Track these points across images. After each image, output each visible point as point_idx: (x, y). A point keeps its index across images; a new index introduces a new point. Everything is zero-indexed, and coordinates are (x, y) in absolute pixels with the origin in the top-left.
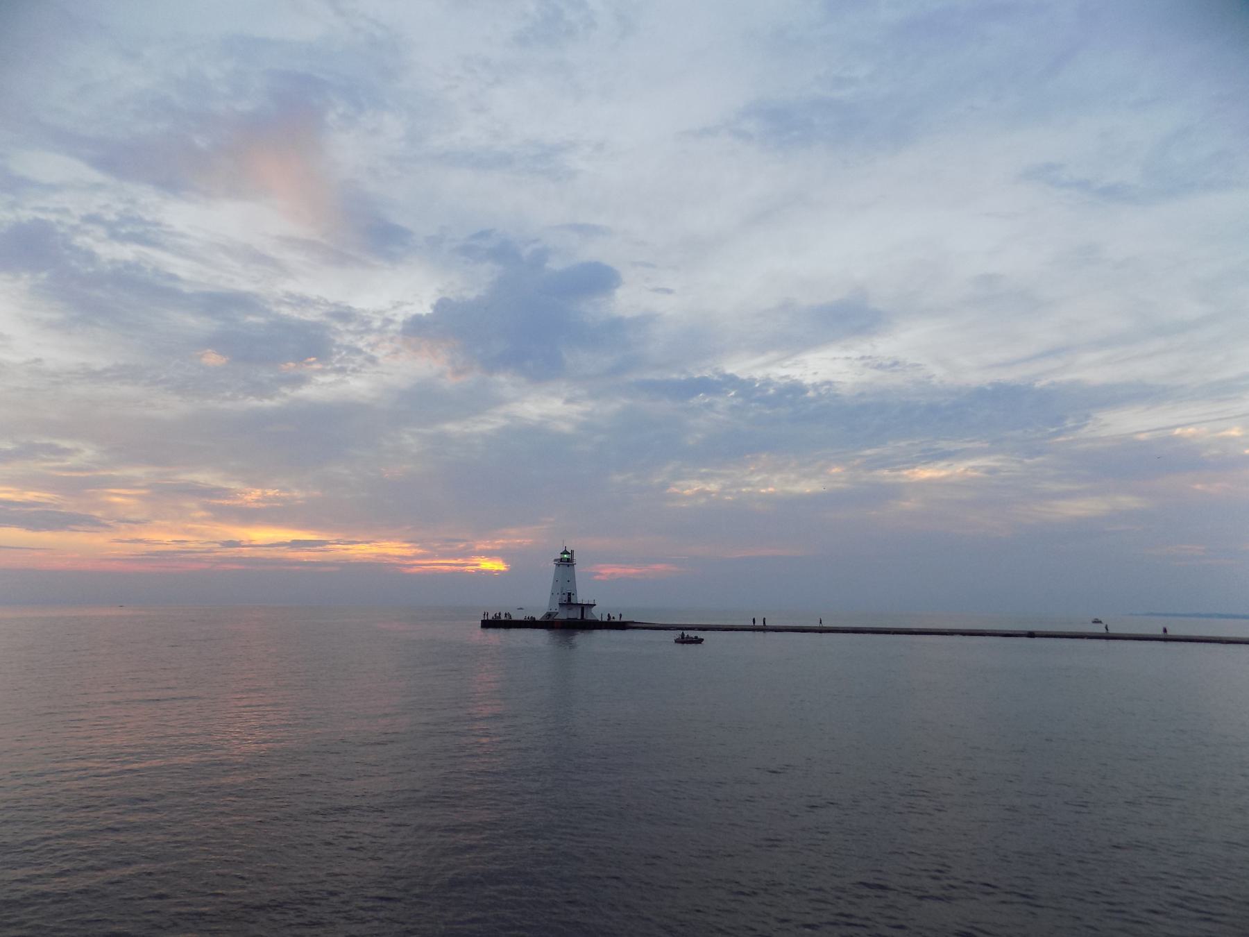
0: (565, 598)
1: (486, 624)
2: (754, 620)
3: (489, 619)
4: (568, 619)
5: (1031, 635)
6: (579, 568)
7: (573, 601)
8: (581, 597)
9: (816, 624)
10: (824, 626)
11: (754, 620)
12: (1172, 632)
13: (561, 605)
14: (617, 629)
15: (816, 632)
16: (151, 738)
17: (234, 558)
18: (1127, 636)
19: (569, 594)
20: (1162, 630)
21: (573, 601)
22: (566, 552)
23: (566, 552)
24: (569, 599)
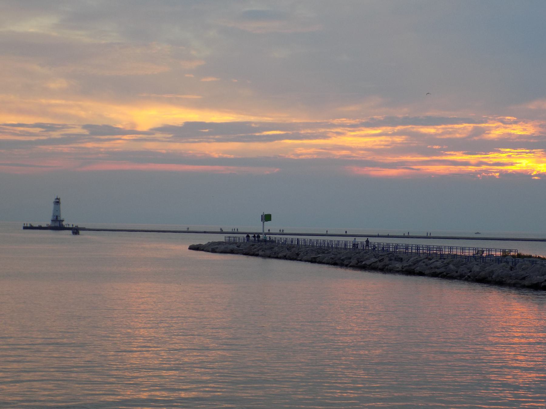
0: (55, 217)
1: (25, 228)
2: (327, 231)
3: (28, 226)
4: (55, 226)
5: (205, 232)
6: (62, 205)
7: (58, 219)
8: (62, 217)
9: (325, 233)
10: (239, 231)
11: (327, 231)
12: (34, 225)
13: (52, 221)
14: (65, 230)
15: (428, 238)
16: (200, 343)
17: (388, 168)
18: (321, 235)
19: (57, 216)
20: (72, 225)
21: (58, 219)
22: (57, 199)
23: (57, 199)
24: (57, 218)
